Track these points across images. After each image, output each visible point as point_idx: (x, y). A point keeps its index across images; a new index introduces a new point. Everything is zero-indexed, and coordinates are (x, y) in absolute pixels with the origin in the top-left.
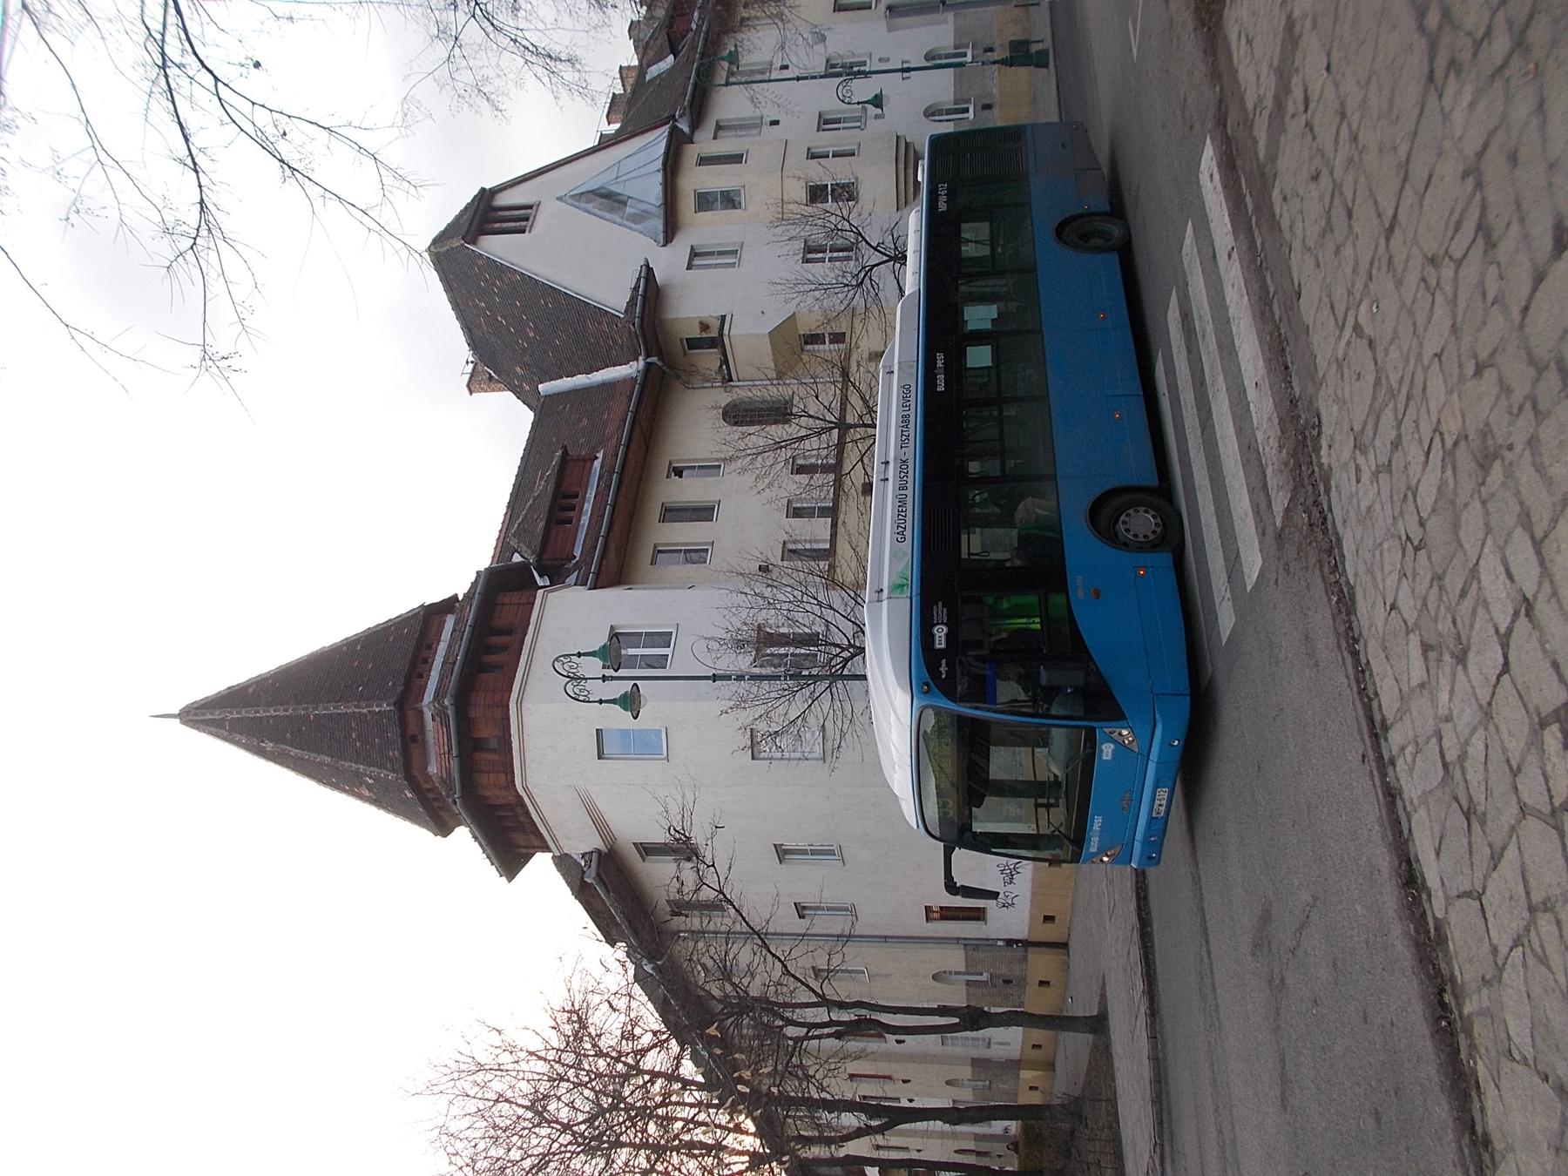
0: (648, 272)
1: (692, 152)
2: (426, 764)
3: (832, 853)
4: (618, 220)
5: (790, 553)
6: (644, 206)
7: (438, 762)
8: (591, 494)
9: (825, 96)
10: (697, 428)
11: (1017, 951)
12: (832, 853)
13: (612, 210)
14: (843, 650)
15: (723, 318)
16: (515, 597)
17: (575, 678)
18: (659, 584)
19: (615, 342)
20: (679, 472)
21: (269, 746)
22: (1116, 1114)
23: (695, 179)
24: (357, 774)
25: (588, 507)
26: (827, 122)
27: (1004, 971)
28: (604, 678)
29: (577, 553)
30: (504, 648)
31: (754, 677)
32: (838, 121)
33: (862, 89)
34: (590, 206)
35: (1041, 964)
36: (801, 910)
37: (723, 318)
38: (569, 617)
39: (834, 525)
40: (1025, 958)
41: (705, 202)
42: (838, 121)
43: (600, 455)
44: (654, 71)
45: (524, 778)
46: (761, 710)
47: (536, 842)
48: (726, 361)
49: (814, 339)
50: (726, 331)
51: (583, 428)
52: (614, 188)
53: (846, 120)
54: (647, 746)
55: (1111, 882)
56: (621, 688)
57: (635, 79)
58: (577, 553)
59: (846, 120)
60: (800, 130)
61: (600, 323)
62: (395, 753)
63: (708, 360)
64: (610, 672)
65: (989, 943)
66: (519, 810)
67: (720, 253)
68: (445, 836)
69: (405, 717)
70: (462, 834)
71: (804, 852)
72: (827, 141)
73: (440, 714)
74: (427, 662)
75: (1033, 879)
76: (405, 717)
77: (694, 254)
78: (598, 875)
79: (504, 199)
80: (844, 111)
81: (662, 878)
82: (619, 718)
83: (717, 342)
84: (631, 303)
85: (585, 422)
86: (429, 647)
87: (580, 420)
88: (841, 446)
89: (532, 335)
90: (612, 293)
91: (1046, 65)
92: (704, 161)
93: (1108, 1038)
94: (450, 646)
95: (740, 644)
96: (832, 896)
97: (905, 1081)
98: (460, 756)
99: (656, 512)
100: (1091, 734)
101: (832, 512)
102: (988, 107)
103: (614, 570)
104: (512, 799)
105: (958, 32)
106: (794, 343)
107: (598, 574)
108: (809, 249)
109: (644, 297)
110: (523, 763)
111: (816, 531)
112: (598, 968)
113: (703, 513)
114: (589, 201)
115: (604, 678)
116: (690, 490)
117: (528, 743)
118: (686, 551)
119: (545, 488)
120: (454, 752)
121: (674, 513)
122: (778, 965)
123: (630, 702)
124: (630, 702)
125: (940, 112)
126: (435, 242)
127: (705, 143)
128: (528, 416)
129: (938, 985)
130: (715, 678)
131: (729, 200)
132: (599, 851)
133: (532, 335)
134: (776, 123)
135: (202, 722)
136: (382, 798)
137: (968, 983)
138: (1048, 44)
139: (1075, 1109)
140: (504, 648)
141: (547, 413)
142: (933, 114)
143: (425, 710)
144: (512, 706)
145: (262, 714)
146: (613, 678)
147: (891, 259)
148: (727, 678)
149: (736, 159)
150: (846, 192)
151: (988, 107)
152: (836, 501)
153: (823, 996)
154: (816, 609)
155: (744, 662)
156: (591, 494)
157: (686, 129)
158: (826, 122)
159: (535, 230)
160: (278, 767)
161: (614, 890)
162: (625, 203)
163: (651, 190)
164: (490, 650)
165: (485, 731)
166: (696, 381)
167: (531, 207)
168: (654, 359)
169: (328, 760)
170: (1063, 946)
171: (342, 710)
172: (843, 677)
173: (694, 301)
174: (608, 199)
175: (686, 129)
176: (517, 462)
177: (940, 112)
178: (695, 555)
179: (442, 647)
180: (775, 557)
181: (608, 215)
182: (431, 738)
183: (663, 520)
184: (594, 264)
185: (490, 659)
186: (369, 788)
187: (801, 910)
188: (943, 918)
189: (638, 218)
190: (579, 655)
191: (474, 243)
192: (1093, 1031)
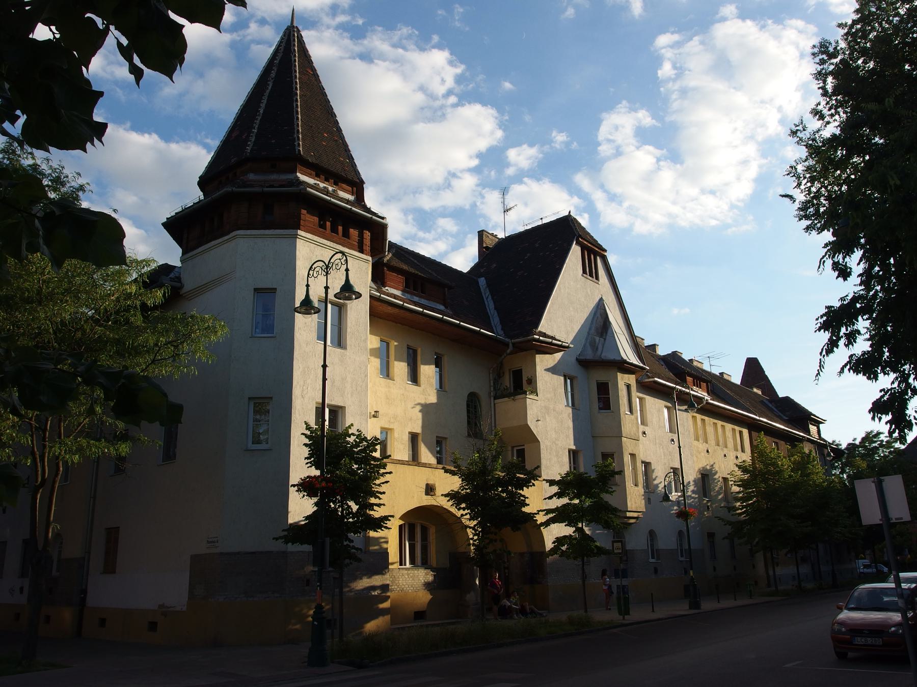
45: (244, 236)
91: (690, 608)
99: (412, 344)
102: (656, 571)
107: (379, 299)
109: (551, 344)
110: (255, 236)
151: (656, 571)
177: (652, 540)
183: (409, 348)
190: (347, 270)
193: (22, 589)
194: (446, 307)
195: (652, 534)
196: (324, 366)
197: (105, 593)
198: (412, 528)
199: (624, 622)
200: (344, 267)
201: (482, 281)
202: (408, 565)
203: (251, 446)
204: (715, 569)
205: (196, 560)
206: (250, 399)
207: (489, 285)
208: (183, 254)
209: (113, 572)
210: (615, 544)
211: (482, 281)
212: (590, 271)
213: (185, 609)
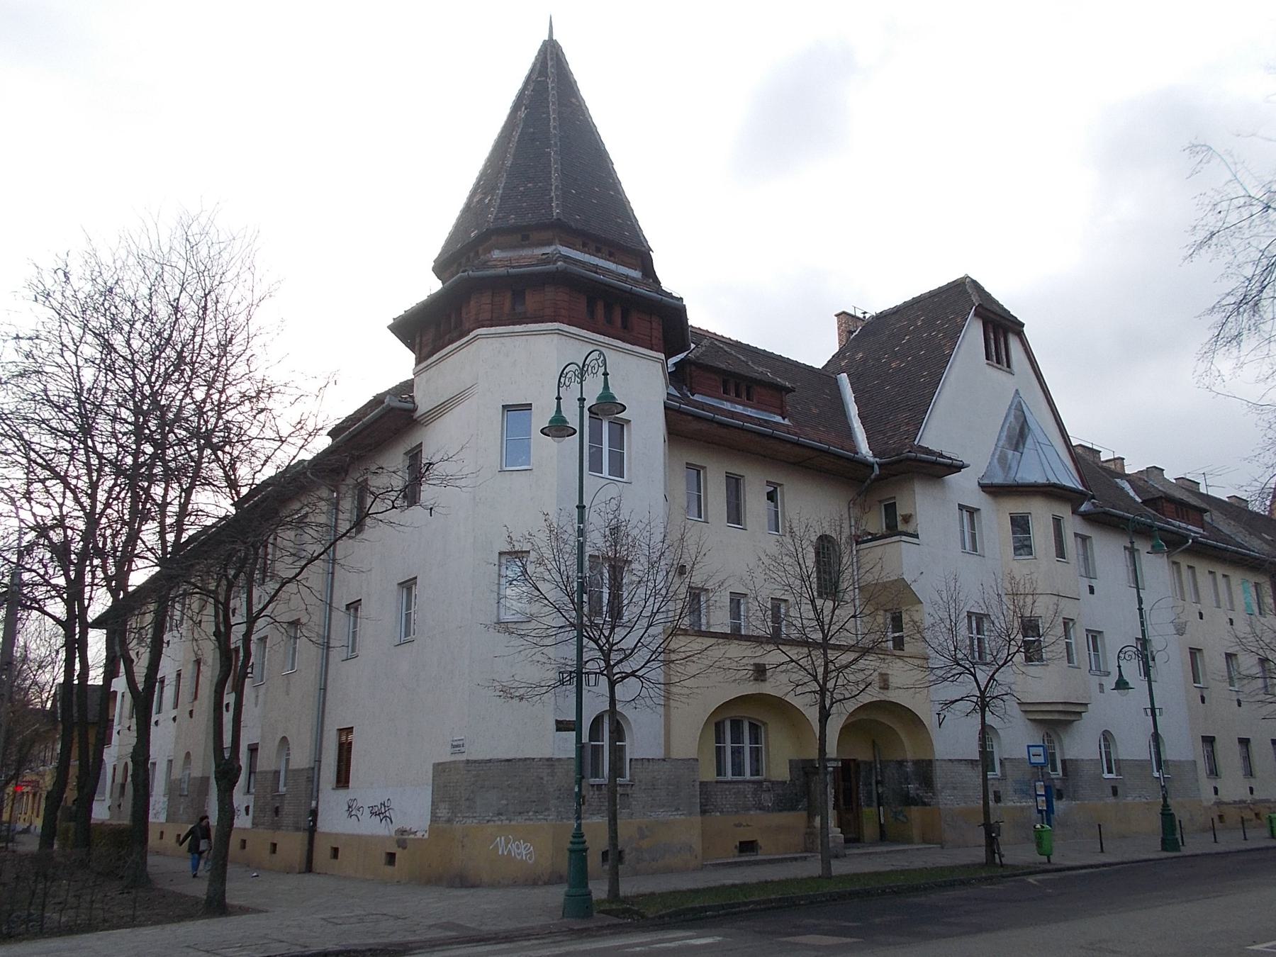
0: (956, 468)
1: (1065, 511)
2: (502, 248)
3: (407, 634)
4: (1001, 443)
5: (695, 594)
6: (1014, 465)
7: (501, 258)
8: (750, 412)
9: (1120, 634)
10: (814, 509)
11: (305, 821)
12: (407, 634)
13: (1009, 438)
14: (607, 639)
15: (916, 536)
16: (657, 333)
17: (582, 373)
18: (669, 467)
19: (890, 438)
20: (771, 497)
21: (522, 114)
22: (118, 927)
23: (1041, 514)
24: (494, 188)
25: (739, 409)
26: (1094, 638)
27: (287, 809)
28: (582, 400)
29: (697, 397)
30: (610, 321)
31: (581, 547)
32: (1096, 649)
33: (1132, 671)
34: (1012, 418)
35: (292, 844)
36: (354, 606)
37: (916, 536)
38: (641, 381)
39: (724, 636)
40: (297, 829)
41: (1020, 524)
42: (1096, 649)
43: (786, 422)
44: (1126, 486)
45: (487, 336)
46: (548, 554)
47: (426, 351)
48: (875, 538)
49: (897, 623)
50: (904, 538)
52: (1029, 441)
53: (1097, 656)
54: (514, 452)
55: (361, 921)
56: (571, 416)
57: (1113, 471)
58: (697, 397)
59: (1097, 656)
60: (1089, 613)
61: (907, 424)
62: (512, 219)
63: (876, 523)
64: (587, 405)
65: (314, 792)
66: (455, 334)
67: (973, 536)
68: (434, 269)
69: (548, 238)
70: (436, 285)
71: (409, 607)
72: (1079, 638)
73: (547, 260)
74: (597, 252)
75: (372, 836)
76: (548, 238)
77: (972, 512)
78: (392, 409)
79: (1014, 344)
80: (1109, 655)
81: (390, 471)
82: (542, 417)
83: (892, 529)
84: (928, 451)
85: (815, 411)
86: (611, 254)
87: (817, 406)
88: (805, 643)
89: (893, 365)
90: (936, 435)
91: (1164, 849)
92: (1057, 521)
93: (200, 918)
94: (612, 272)
95: (615, 530)
96: (367, 629)
97: (191, 712)
98: (509, 276)
99: (736, 470)
100: (1271, 512)
101: (735, 635)
102: (1115, 792)
103: (682, 429)
104: (467, 325)
105: (1178, 764)
106: (894, 604)
107: (679, 411)
108: (980, 618)
109: (935, 463)
110: (501, 335)
111: (719, 620)
113: (735, 515)
114: (1016, 417)
115: (582, 400)
117: (519, 341)
118: (699, 497)
119: (757, 372)
120: (511, 270)
121: (734, 486)
122: (291, 574)
123: (557, 428)
124: (557, 428)
125: (1107, 747)
126: (974, 282)
127: (1072, 525)
128: (819, 364)
130: (581, 507)
131: (1023, 546)
132: (415, 410)
133: (893, 365)
134: (1092, 590)
136: (471, 212)
137: (277, 773)
138: (1185, 851)
139: (139, 879)
140: (610, 321)
141: (823, 379)
142: (1105, 739)
143: (553, 248)
144: (556, 325)
145: (551, 107)
146: (582, 408)
147: (982, 693)
148: (581, 519)
149: (1061, 553)
150: (1033, 653)
151: (1115, 792)
152: (748, 638)
153: (258, 617)
154: (647, 613)
155: (597, 541)
156: (750, 412)
157: (1083, 508)
158: (1094, 636)
159: (990, 370)
160: (502, 123)
161: (383, 429)
162: (1016, 449)
163: (1030, 473)
164: (609, 308)
165: (531, 301)
166: (856, 512)
167: (1009, 366)
169: (508, 163)
170: (309, 868)
171: (554, 175)
172: (580, 637)
173: (930, 509)
174: (1019, 434)
175: (1083, 508)
177: (1107, 747)
178: (699, 507)
179: (611, 266)
180: (697, 580)
181: (1005, 434)
182: (524, 253)
183: (729, 476)
184: (963, 415)
186: (482, 200)
187: (354, 606)
188: (341, 745)
189: (1003, 460)
190: (606, 374)
191: (976, 315)
192: (209, 901)
193: (247, 808)
195: (1107, 737)
197: (335, 817)
198: (719, 727)
199: (1049, 867)
200: (602, 370)
202: (748, 776)
204: (1251, 790)
206: (500, 554)
208: (418, 362)
210: (1033, 750)
212: (997, 354)
213: (426, 836)
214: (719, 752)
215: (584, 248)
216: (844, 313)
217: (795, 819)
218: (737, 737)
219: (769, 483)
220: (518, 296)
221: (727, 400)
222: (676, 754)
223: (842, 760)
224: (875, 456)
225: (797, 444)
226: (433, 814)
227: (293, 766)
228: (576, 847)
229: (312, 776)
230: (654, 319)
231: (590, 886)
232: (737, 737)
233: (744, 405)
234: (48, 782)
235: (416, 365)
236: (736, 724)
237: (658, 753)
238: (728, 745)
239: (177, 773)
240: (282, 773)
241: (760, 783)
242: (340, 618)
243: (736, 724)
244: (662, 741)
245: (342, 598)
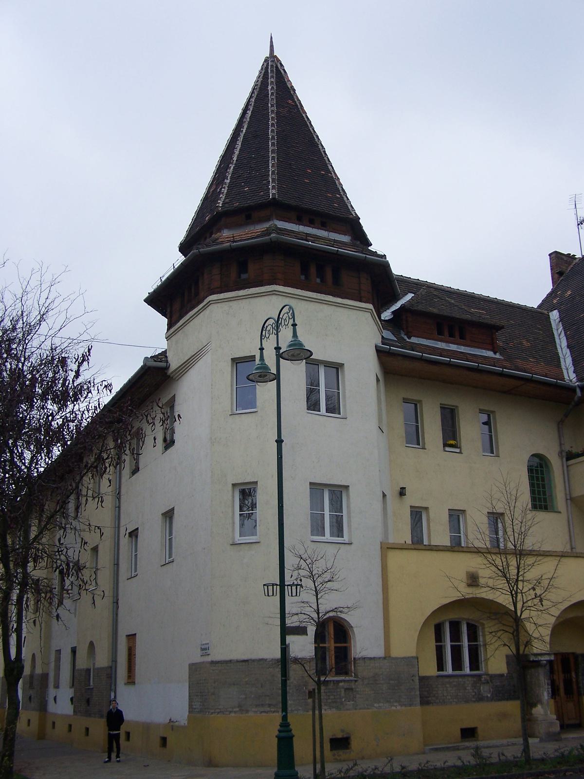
2: (229, 227)
7: (228, 237)
8: (462, 349)
29: (414, 340)
38: (347, 333)
43: (498, 356)
51: (521, 343)
69: (272, 210)
70: (181, 258)
71: (171, 533)
76: (272, 210)
87: (528, 341)
99: (450, 401)
101: (456, 547)
103: (394, 367)
107: (389, 353)
111: (439, 534)
112: (110, 373)
116: (470, 429)
129: (87, 645)
132: (167, 368)
135: (267, 68)
143: (271, 223)
149: (59, 652)
156: (462, 349)
161: (153, 383)
165: (253, 268)
168: (578, 390)
176: (493, 295)
178: (416, 438)
180: (412, 499)
183: (443, 408)
185: (313, 270)
194: (495, 353)
196: (279, 442)
198: (439, 629)
200: (291, 322)
201: (554, 315)
202: (467, 670)
203: (238, 539)
205: (194, 668)
206: (234, 485)
207: (562, 320)
209: (133, 683)
211: (554, 315)
214: (440, 651)
215: (299, 221)
216: (556, 252)
217: (513, 707)
218: (456, 636)
219: (481, 411)
220: (243, 267)
221: (441, 341)
222: (396, 652)
223: (555, 654)
224: (579, 380)
225: (502, 374)
226: (191, 706)
227: (96, 666)
228: (283, 734)
229: (110, 673)
230: (362, 276)
231: (296, 769)
232: (456, 636)
233: (457, 344)
234: (485, 593)
235: (168, 330)
236: (455, 626)
237: (379, 652)
238: (448, 644)
239: (82, 662)
240: (92, 670)
241: (479, 676)
242: (124, 541)
243: (455, 626)
244: (382, 643)
245: (128, 524)
